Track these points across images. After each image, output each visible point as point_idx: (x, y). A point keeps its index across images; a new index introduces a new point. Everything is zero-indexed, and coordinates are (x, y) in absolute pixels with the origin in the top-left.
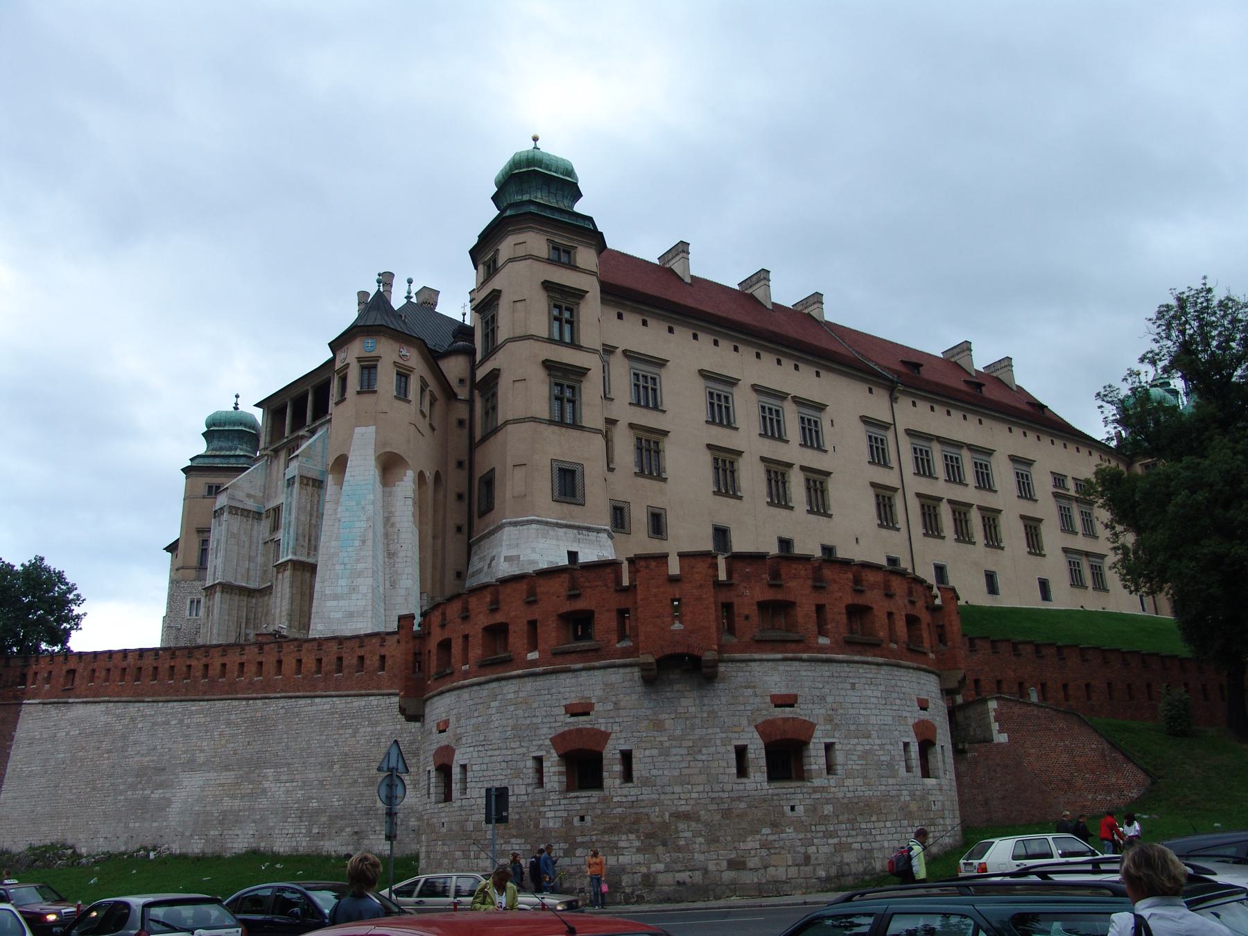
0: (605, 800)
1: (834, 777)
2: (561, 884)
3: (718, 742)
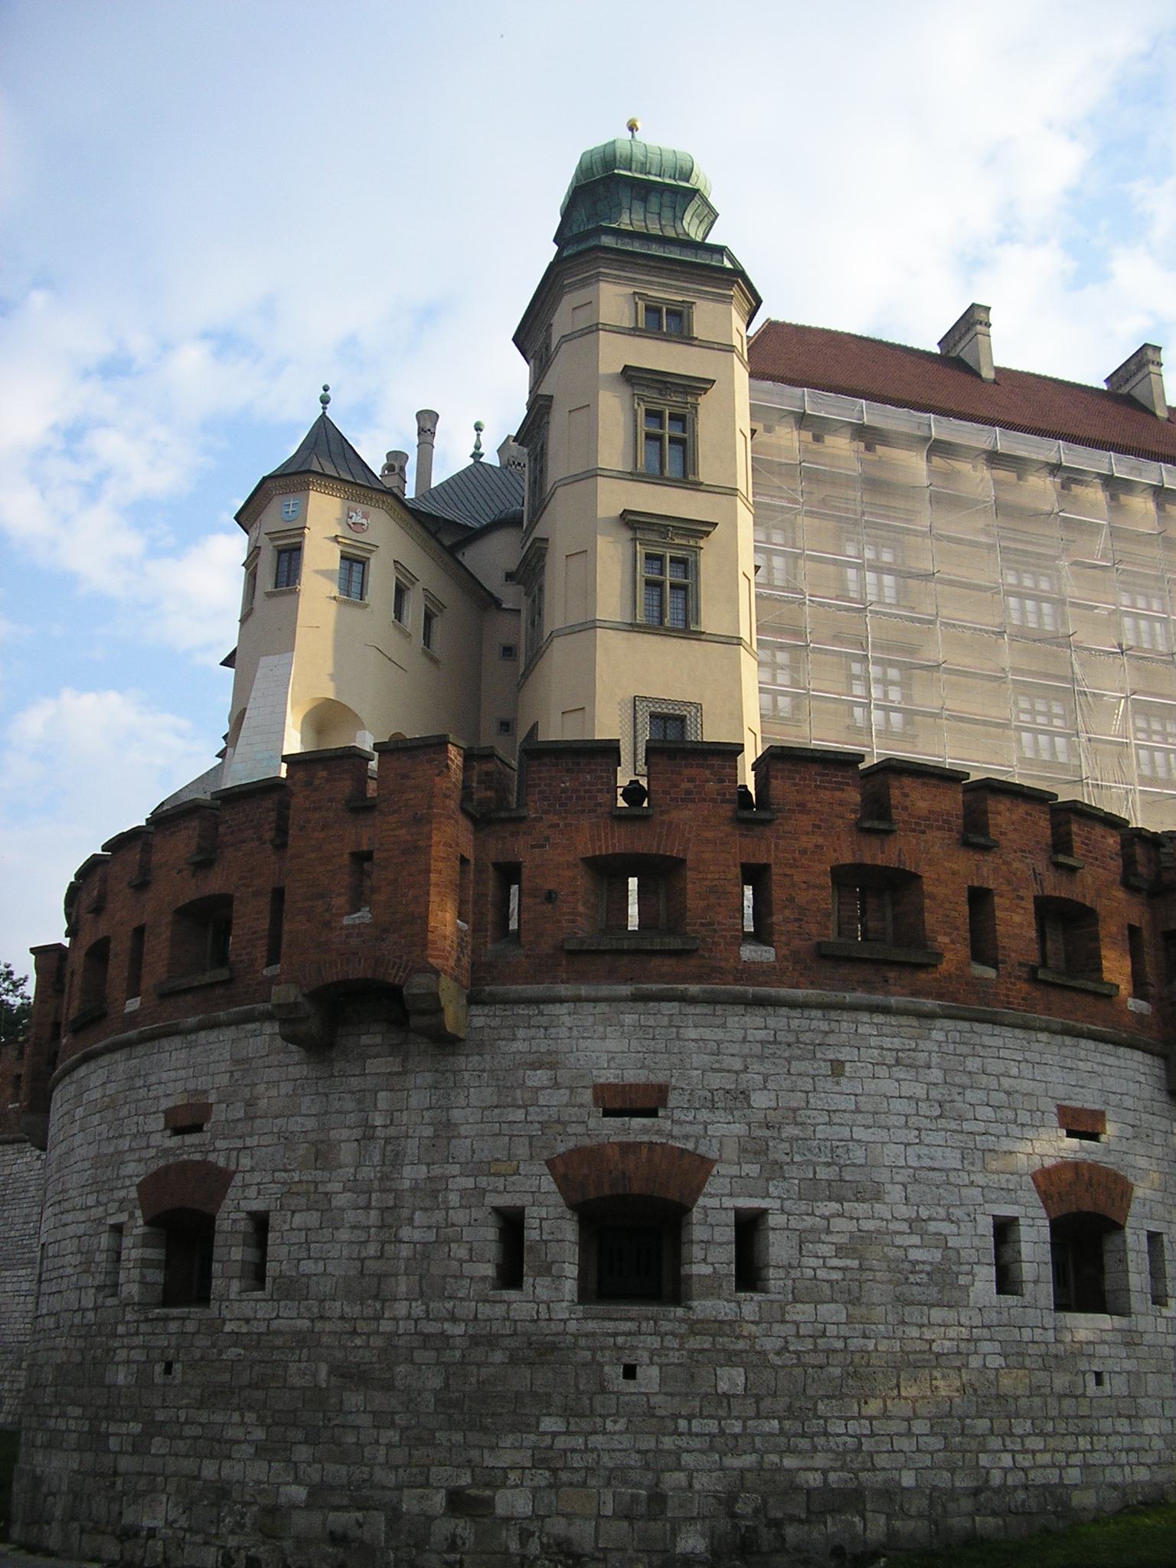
0: (213, 1328)
1: (757, 1297)
2: (121, 1514)
3: (454, 1199)
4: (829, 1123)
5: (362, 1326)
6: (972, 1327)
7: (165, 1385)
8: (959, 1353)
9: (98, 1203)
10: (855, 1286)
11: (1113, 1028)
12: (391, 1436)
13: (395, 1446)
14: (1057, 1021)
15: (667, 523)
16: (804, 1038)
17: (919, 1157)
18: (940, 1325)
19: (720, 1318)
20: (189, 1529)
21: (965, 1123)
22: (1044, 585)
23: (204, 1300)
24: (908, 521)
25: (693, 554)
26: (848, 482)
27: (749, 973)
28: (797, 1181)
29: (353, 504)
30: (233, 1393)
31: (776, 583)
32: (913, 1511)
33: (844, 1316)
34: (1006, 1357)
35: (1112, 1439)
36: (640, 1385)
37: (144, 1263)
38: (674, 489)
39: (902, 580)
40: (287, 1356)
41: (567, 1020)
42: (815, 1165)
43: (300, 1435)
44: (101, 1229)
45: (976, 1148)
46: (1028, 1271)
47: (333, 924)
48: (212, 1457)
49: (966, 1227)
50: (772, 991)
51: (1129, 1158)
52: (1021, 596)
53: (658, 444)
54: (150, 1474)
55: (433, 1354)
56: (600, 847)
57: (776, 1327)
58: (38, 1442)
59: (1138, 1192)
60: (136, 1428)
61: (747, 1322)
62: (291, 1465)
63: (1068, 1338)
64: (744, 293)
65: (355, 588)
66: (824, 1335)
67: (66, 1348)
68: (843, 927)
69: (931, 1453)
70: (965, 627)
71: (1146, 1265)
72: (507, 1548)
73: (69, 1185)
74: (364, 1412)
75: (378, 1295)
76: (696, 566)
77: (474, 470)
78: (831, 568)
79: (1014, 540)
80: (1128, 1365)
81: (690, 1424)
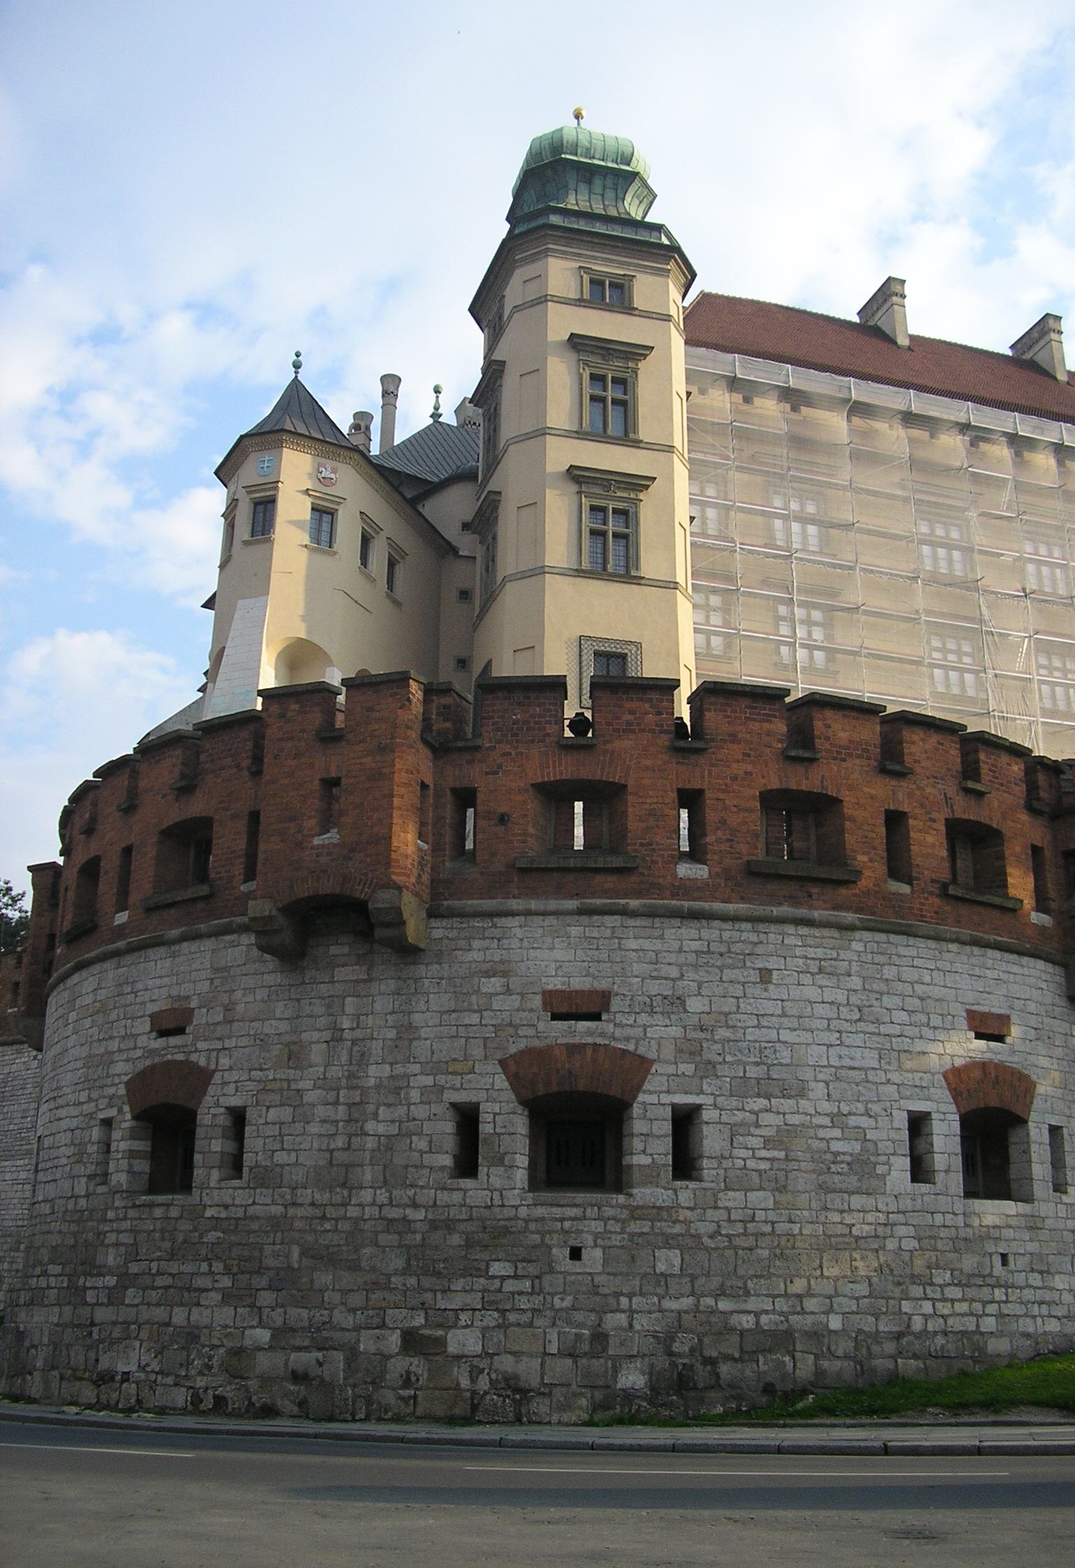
0: (195, 1213)
1: (692, 1185)
2: (97, 1360)
3: (415, 1095)
4: (758, 1026)
6: (888, 1213)
8: (876, 1236)
9: (90, 1100)
10: (781, 1175)
11: (1017, 939)
14: (966, 933)
17: (840, 1057)
18: (859, 1211)
19: (658, 1204)
20: (161, 1372)
21: (882, 1026)
22: (954, 534)
23: (186, 1187)
24: (830, 475)
25: (634, 506)
28: (728, 1079)
29: (323, 460)
31: (710, 532)
32: (840, 1353)
33: (772, 1202)
34: (919, 1240)
35: (1026, 1291)
36: (585, 1266)
37: (132, 1154)
39: (824, 530)
41: (519, 932)
42: (745, 1064)
44: (93, 1123)
46: (939, 1161)
47: (305, 844)
48: (182, 1305)
49: (883, 1122)
50: (705, 905)
51: (1032, 1059)
52: (934, 544)
53: (601, 405)
54: (124, 1323)
56: (549, 774)
57: (710, 1213)
58: (22, 1301)
59: (1041, 1089)
61: (683, 1208)
62: (256, 1310)
63: (976, 1222)
64: (680, 267)
65: (325, 537)
66: (753, 1220)
67: (60, 1232)
68: (770, 846)
69: (857, 1299)
70: (881, 572)
72: (458, 1384)
73: (63, 1083)
76: (637, 517)
77: (433, 429)
78: (760, 519)
79: (927, 493)
81: (630, 1301)
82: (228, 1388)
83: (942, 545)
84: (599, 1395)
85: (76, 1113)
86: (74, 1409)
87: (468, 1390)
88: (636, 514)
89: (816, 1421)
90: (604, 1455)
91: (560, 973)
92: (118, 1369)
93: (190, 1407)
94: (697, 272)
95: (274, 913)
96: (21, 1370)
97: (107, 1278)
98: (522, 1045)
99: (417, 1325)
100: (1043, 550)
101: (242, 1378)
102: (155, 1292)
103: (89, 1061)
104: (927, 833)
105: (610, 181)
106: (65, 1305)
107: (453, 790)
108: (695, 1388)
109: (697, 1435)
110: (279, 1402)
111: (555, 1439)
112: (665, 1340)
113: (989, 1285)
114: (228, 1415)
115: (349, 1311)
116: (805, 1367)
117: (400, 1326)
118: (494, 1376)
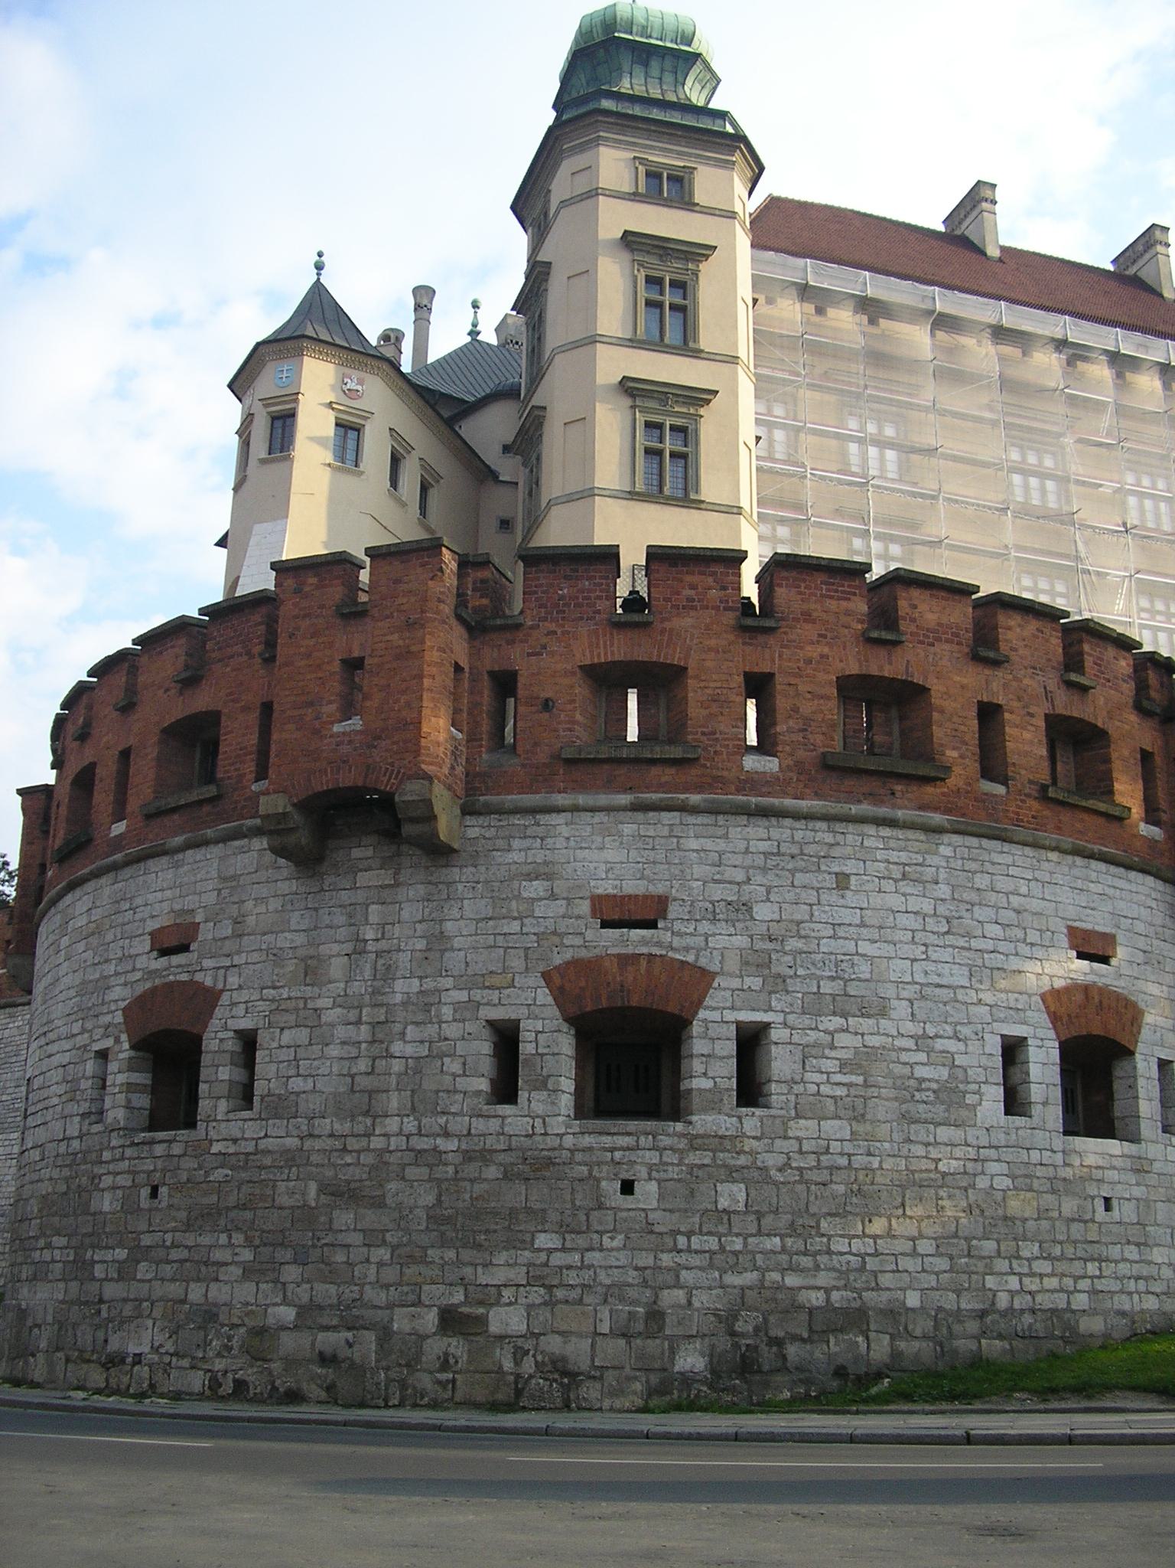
0: (201, 1149)
1: (758, 1112)
2: (106, 1341)
3: (447, 1012)
4: (834, 937)
5: (353, 1144)
6: (979, 1147)
7: (150, 1210)
8: (965, 1173)
9: (84, 1031)
10: (859, 1102)
11: (1126, 851)
12: (383, 1253)
13: (386, 1264)
14: (1067, 842)
15: (666, 390)
16: (808, 850)
17: (926, 973)
18: (947, 1145)
19: (720, 1133)
20: (176, 1354)
21: (972, 940)
22: (1048, 462)
23: (191, 1124)
24: (910, 395)
25: (693, 422)
26: (849, 355)
27: (751, 783)
28: (800, 995)
29: (348, 371)
30: (220, 1214)
31: (778, 456)
32: (918, 1332)
33: (849, 1132)
34: (1014, 1178)
35: (1121, 1265)
36: (639, 1201)
37: (130, 1087)
38: (674, 357)
39: (904, 455)
40: (275, 1175)
41: (565, 831)
42: (819, 979)
43: (289, 1255)
44: (86, 1056)
45: (984, 966)
46: (1036, 1093)
47: (324, 732)
48: (198, 1280)
49: (974, 1046)
50: (776, 801)
51: (1140, 984)
52: (1025, 472)
53: (658, 311)
54: (136, 1300)
55: (425, 1170)
56: (599, 655)
57: (778, 1142)
58: (24, 1276)
59: (1148, 1019)
60: (121, 1254)
61: (749, 1137)
62: (279, 1286)
63: (1077, 1162)
64: (746, 159)
65: (350, 455)
66: (827, 1151)
67: (51, 1179)
68: (848, 740)
69: (937, 1274)
70: (967, 503)
71: (1156, 1092)
72: (501, 1367)
73: (53, 1016)
74: (355, 1230)
75: (368, 1111)
76: (697, 435)
77: (471, 347)
78: (833, 443)
79: (1020, 416)
80: (1138, 1192)
81: (689, 1240)
82: (250, 1371)
83: (1035, 474)
84: (654, 1379)
85: (67, 1047)
86: (81, 1394)
87: (512, 1373)
88: (696, 431)
89: (892, 1407)
90: (661, 1444)
91: (610, 876)
92: (129, 1350)
93: (208, 1392)
94: (765, 165)
95: (289, 809)
96: (23, 1351)
97: (117, 1250)
98: (568, 955)
99: (456, 1302)
100: (1146, 482)
101: (265, 1360)
102: (169, 1266)
103: (83, 988)
104: (1024, 728)
105: (668, 63)
106: (71, 1280)
107: (491, 674)
108: (760, 1371)
109: (762, 1422)
110: (305, 1386)
111: (607, 1427)
112: (727, 1318)
113: (1081, 1258)
114: (250, 1401)
115: (382, 1287)
116: (879, 1348)
117: (437, 1303)
118: (539, 1358)
